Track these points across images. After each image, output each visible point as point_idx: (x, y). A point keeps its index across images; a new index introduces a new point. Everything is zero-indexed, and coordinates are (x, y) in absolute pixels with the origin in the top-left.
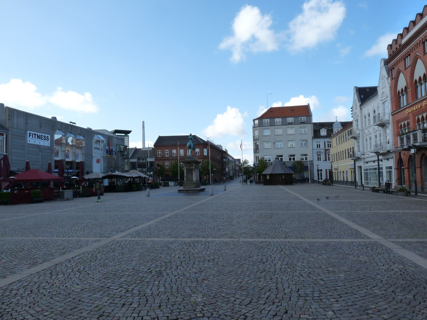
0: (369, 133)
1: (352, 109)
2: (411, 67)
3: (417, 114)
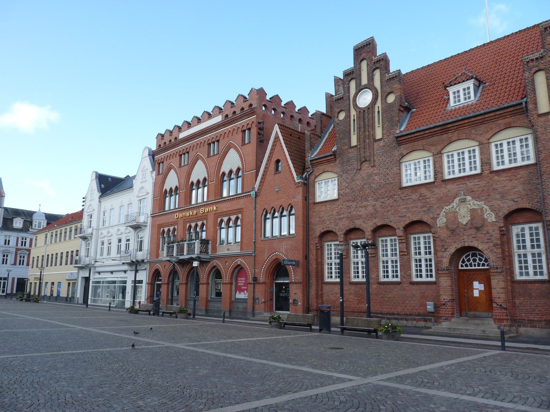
0: (110, 235)
1: (84, 200)
2: (162, 175)
3: (189, 221)
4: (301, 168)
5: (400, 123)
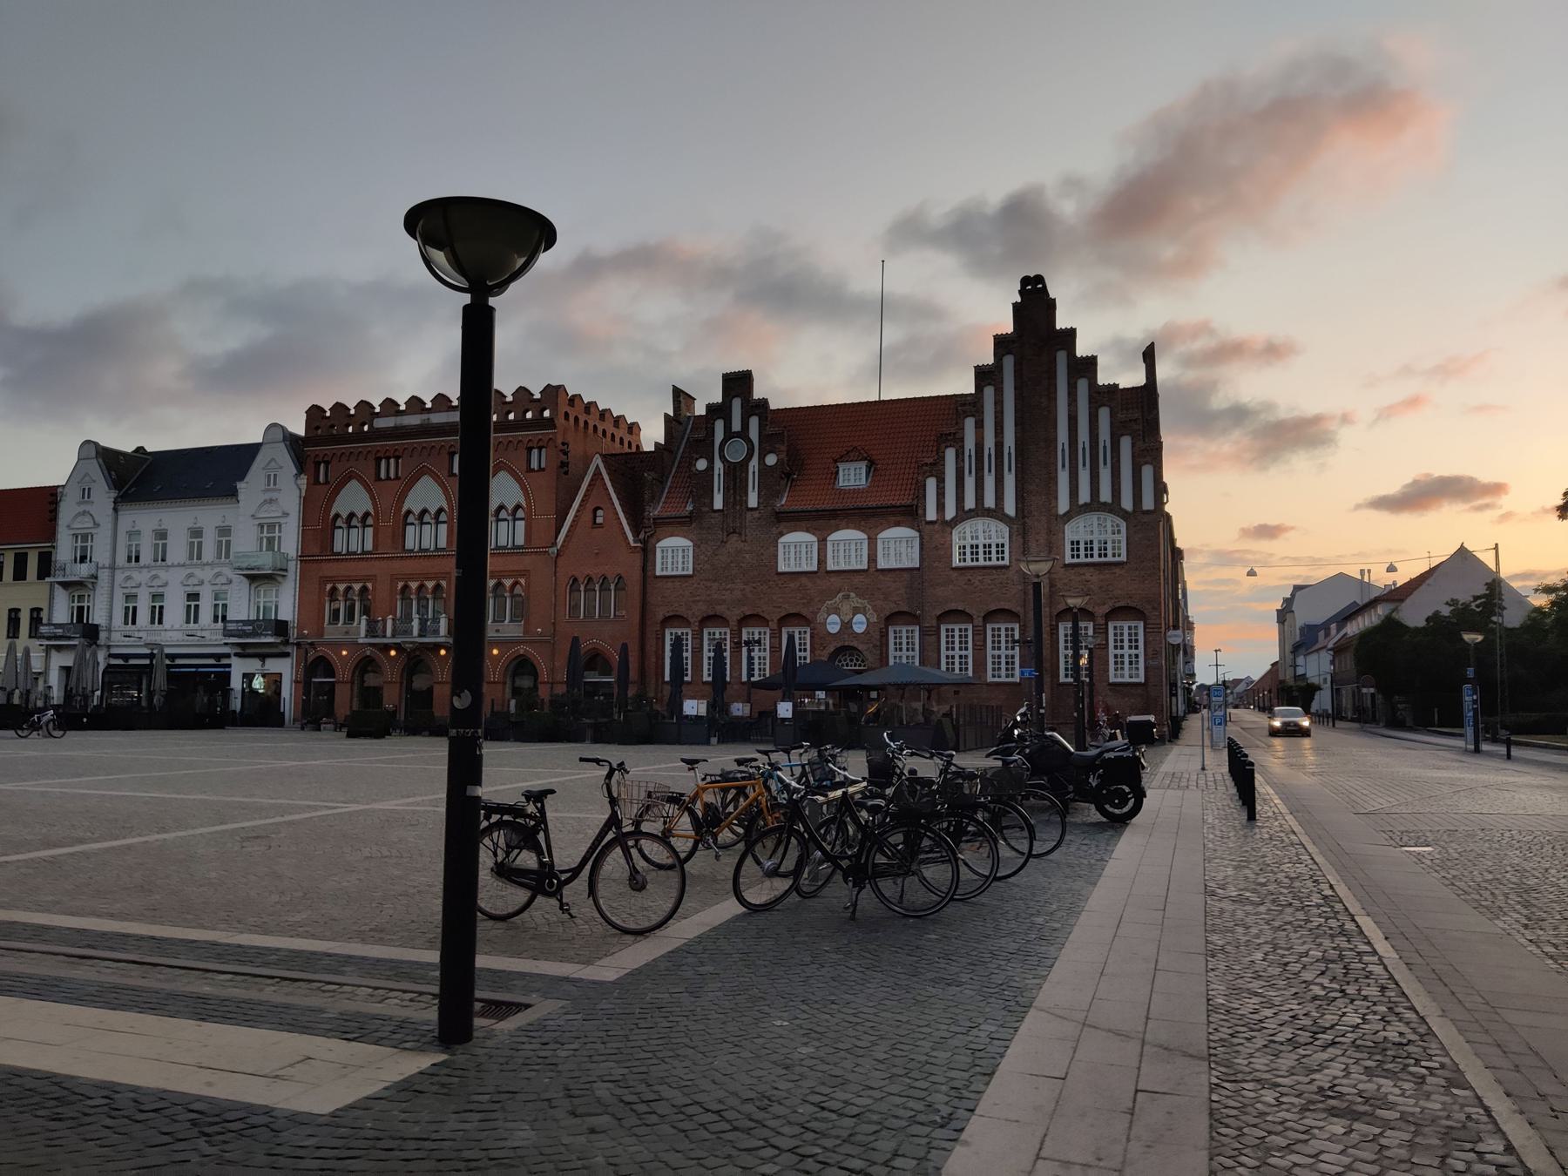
4: (636, 527)
5: (778, 495)
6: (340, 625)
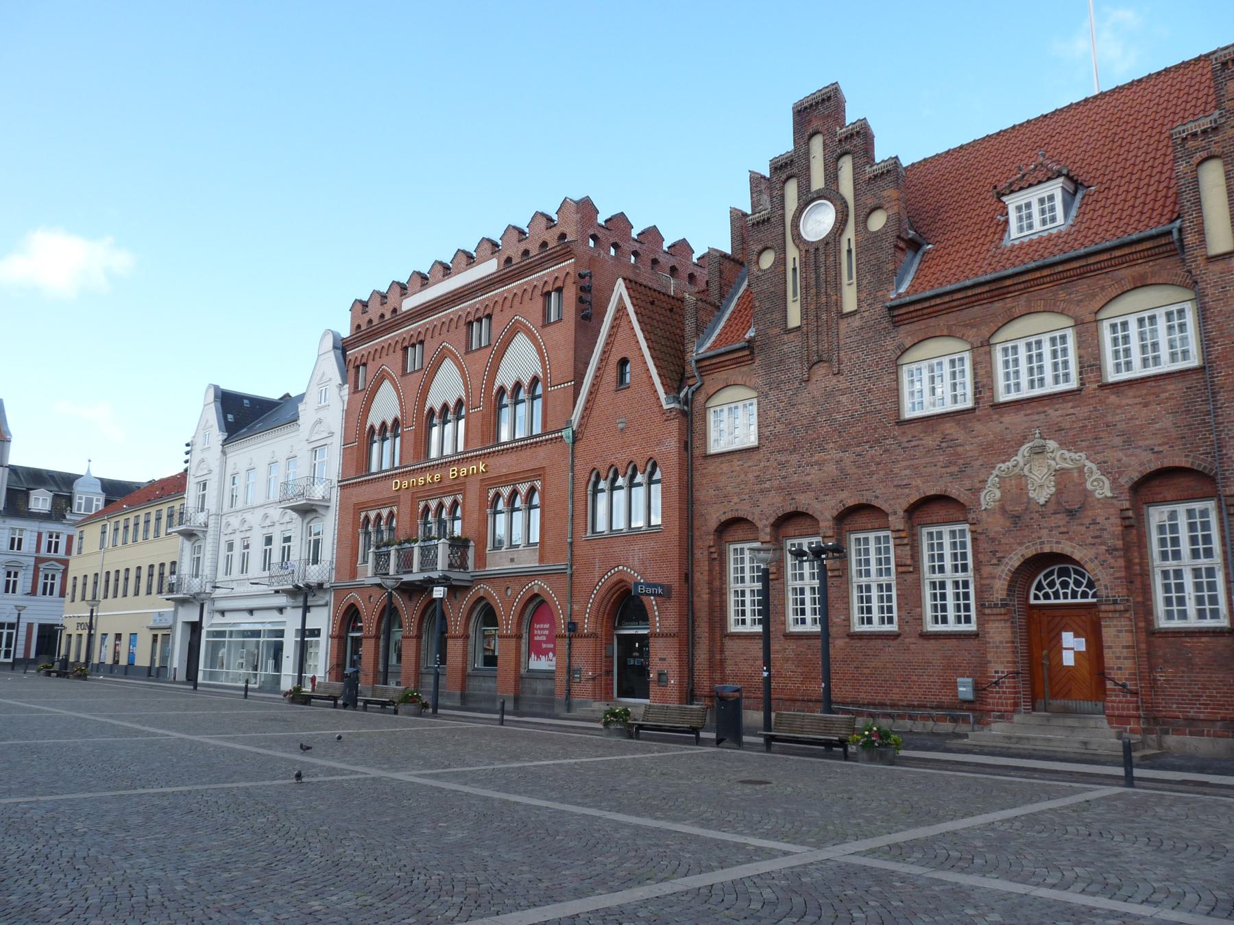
0: (246, 527)
1: (189, 448)
2: (364, 393)
3: (424, 497)
4: (676, 377)
5: (897, 275)
6: (503, 549)
